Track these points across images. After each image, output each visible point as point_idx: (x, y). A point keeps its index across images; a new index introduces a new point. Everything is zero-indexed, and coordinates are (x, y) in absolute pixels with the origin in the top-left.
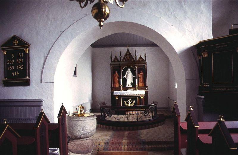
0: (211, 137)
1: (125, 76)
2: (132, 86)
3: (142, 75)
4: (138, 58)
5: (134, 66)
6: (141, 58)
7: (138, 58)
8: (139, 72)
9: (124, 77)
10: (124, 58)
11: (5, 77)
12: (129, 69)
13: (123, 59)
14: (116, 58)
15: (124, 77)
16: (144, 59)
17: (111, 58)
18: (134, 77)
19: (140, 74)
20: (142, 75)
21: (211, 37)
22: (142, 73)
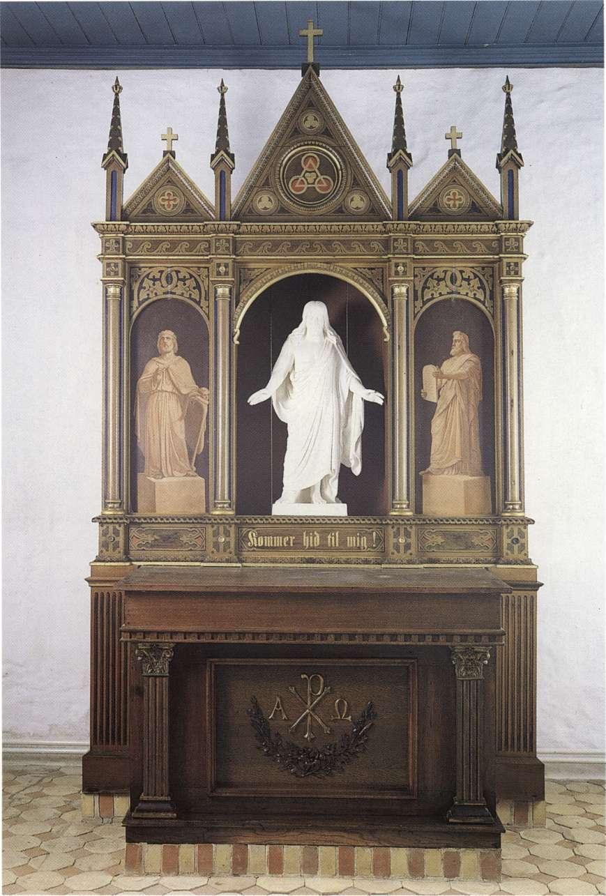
0: (346, 505)
1: (269, 392)
2: (341, 510)
3: (462, 381)
4: (418, 183)
5: (381, 280)
6: (456, 173)
7: (418, 183)
8: (429, 349)
9: (256, 399)
10: (262, 179)
11: (105, 505)
12: (315, 314)
13: (252, 189)
14: (168, 174)
15: (256, 399)
16: (493, 186)
17: (116, 160)
18: (368, 405)
19: (439, 376)
20: (462, 381)
21: (128, 799)
22: (461, 362)
